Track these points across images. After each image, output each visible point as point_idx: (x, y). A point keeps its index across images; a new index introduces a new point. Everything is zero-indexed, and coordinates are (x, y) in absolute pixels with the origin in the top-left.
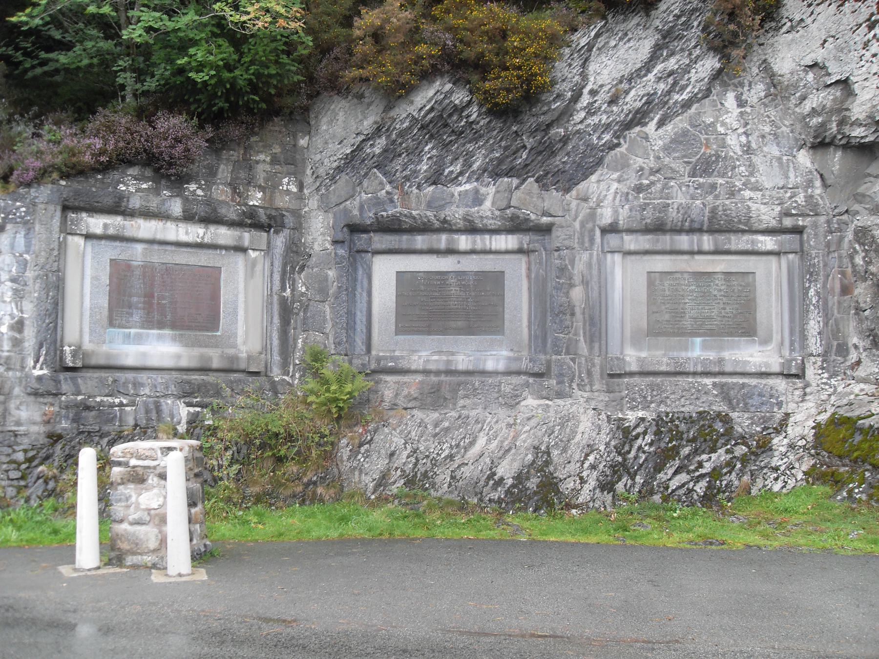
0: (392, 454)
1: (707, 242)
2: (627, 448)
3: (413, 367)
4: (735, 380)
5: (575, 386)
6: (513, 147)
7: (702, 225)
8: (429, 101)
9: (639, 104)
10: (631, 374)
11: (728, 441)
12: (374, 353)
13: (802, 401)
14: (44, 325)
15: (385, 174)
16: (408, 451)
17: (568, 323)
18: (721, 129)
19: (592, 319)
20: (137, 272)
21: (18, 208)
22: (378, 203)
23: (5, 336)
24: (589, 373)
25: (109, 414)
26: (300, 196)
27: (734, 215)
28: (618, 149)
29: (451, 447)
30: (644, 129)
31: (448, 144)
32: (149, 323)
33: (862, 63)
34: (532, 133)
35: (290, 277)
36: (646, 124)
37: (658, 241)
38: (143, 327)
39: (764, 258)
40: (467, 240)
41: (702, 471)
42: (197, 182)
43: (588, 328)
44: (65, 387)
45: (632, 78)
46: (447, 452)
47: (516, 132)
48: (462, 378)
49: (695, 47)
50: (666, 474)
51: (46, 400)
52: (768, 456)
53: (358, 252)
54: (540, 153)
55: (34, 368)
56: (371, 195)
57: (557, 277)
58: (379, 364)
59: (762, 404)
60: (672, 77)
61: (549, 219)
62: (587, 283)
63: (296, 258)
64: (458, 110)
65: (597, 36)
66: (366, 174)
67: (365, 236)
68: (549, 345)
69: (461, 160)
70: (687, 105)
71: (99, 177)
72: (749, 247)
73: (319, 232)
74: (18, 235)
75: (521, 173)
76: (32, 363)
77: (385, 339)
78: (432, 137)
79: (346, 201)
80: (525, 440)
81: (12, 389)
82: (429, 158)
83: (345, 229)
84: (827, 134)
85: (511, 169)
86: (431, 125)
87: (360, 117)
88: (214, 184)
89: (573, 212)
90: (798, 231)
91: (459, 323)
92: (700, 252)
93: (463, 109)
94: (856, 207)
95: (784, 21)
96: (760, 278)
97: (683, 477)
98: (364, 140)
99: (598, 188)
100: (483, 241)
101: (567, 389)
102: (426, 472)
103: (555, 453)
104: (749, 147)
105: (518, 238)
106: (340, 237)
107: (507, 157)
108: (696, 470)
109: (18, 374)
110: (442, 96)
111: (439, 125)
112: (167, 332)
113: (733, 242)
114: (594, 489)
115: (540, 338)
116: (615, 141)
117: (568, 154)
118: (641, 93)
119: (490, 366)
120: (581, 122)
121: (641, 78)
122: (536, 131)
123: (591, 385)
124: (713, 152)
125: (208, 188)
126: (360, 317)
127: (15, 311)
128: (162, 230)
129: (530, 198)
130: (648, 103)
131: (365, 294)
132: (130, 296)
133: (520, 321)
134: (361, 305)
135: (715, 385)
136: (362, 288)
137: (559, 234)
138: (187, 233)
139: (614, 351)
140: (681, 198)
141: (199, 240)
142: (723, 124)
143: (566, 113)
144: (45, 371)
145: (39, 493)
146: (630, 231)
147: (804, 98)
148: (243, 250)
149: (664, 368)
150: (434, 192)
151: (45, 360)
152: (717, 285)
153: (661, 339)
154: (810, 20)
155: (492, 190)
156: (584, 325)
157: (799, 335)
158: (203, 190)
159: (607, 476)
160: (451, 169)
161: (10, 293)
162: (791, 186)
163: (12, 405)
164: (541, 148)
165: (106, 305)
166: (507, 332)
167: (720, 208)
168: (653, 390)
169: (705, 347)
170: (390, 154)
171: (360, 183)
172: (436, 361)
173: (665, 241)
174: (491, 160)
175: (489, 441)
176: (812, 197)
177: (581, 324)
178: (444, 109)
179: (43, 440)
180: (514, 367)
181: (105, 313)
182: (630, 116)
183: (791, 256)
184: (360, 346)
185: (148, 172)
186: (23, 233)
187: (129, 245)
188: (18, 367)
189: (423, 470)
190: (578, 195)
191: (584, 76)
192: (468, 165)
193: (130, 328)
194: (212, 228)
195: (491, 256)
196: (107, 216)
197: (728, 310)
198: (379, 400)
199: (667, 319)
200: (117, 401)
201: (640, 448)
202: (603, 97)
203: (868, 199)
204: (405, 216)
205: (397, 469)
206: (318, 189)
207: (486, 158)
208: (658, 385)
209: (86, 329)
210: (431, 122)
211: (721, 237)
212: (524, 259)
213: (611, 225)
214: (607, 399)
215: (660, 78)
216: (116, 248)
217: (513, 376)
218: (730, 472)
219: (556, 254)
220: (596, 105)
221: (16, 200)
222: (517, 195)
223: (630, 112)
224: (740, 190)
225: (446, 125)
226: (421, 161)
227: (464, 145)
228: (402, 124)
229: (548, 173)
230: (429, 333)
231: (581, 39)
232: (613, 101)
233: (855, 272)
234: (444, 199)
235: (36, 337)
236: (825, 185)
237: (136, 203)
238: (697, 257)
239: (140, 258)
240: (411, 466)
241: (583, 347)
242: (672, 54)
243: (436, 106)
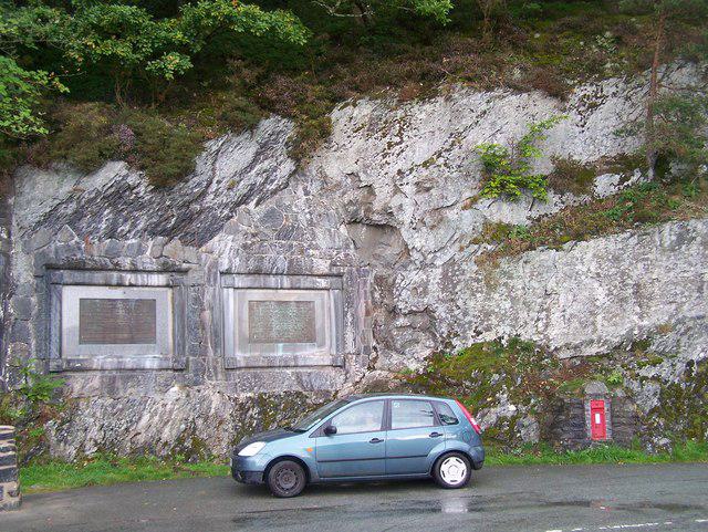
1: (286, 282)
9: (246, 191)
10: (240, 368)
22: (68, 248)
24: (215, 368)
64: (131, 188)
70: (274, 192)
75: (170, 234)
77: (72, 348)
90: (340, 275)
92: (281, 288)
96: (318, 303)
111: (118, 196)
115: (179, 346)
119: (148, 364)
126: (54, 331)
129: (176, 250)
134: (55, 323)
139: (229, 354)
142: (296, 206)
147: (344, 193)
149: (261, 364)
153: (258, 345)
154: (349, 146)
155: (150, 243)
157: (341, 341)
166: (158, 342)
169: (284, 349)
170: (78, 215)
172: (110, 363)
175: (152, 417)
180: (165, 365)
192: (134, 225)
195: (147, 289)
199: (260, 336)
206: (22, 237)
212: (170, 291)
222: (168, 247)
225: (120, 198)
227: (131, 212)
230: (104, 343)
231: (213, 145)
233: (374, 302)
236: (356, 248)
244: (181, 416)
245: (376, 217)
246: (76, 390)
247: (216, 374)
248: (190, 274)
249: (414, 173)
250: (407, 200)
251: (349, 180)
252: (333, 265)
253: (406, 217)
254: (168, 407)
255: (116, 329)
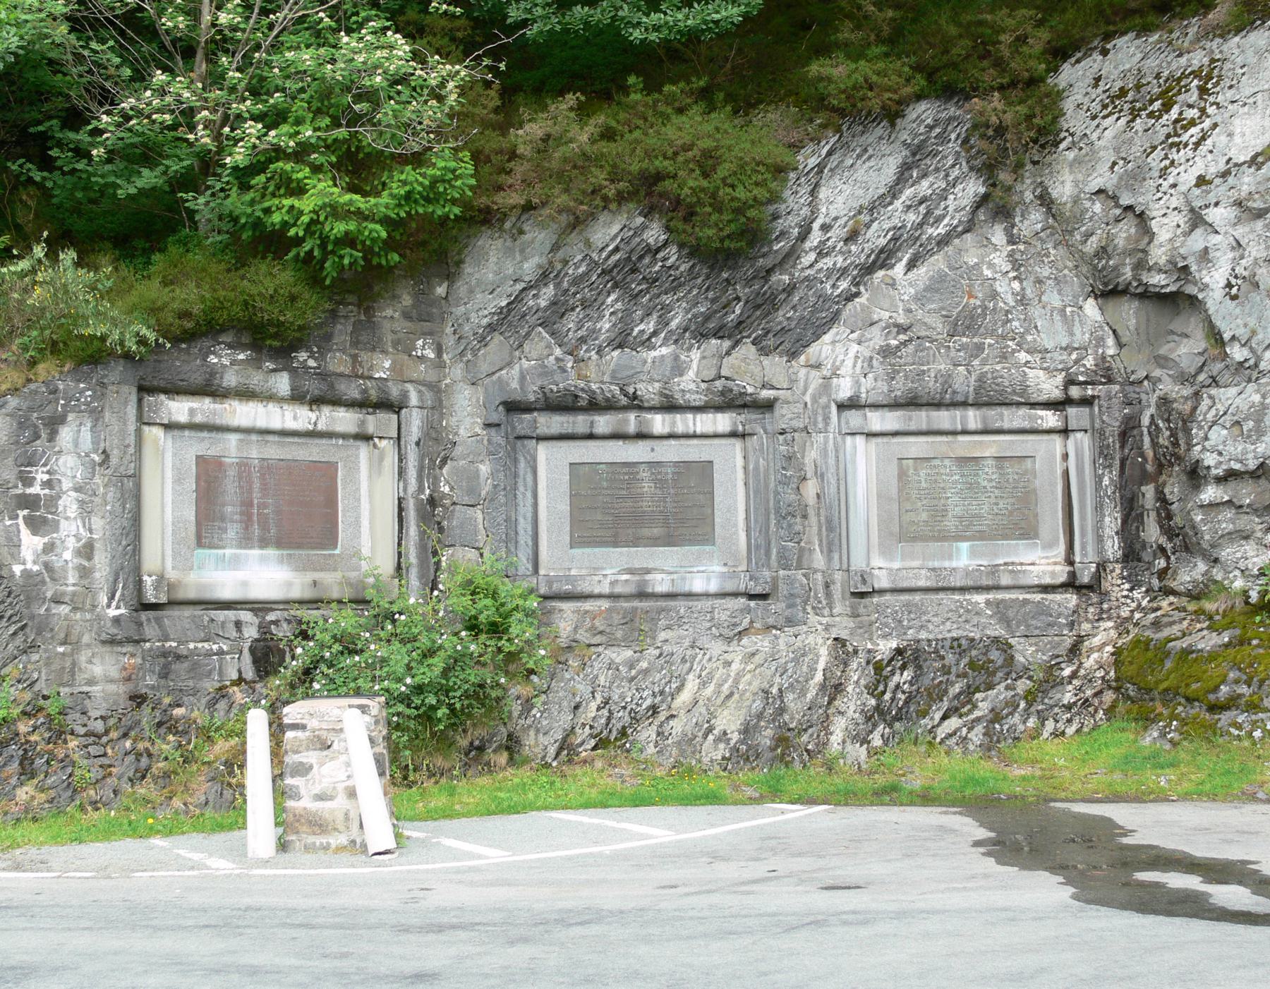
0: (576, 707)
1: (973, 418)
2: (881, 688)
3: (597, 591)
4: (1013, 596)
5: (809, 609)
6: (724, 300)
7: (967, 397)
8: (613, 239)
9: (882, 242)
10: (882, 592)
11: (1008, 674)
12: (542, 572)
13: (1098, 620)
14: (121, 548)
15: (552, 334)
16: (599, 699)
17: (798, 528)
18: (988, 273)
19: (829, 521)
20: (232, 473)
21: (82, 392)
23: (70, 565)
25: (208, 665)
26: (439, 364)
27: (1007, 384)
28: (857, 300)
29: (654, 695)
30: (890, 272)
31: (637, 295)
32: (246, 541)
33: (1159, 195)
34: (748, 282)
35: (429, 473)
36: (892, 267)
37: (910, 419)
38: (240, 547)
39: (1046, 437)
40: (664, 421)
41: (977, 713)
42: (309, 349)
43: (824, 533)
44: (150, 631)
45: (874, 207)
46: (648, 702)
47: (727, 280)
48: (662, 603)
49: (953, 166)
50: (932, 719)
51: (124, 650)
52: (1059, 692)
53: (519, 438)
54: (758, 307)
55: (109, 606)
56: (533, 363)
57: (784, 468)
58: (550, 588)
59: (1049, 625)
60: (924, 205)
61: (771, 392)
62: (822, 475)
63: (437, 450)
65: (830, 154)
66: (528, 334)
67: (527, 416)
68: (774, 557)
69: (655, 316)
70: (943, 241)
71: (184, 346)
72: (1026, 425)
73: (467, 415)
74: (83, 428)
75: (733, 333)
76: (106, 600)
78: (616, 286)
79: (501, 369)
80: (751, 684)
81: (81, 635)
82: (612, 314)
83: (501, 408)
84: (1120, 280)
85: (721, 328)
86: (615, 271)
87: (518, 257)
88: (330, 350)
89: (802, 383)
91: (655, 530)
92: (965, 432)
93: (658, 250)
94: (1157, 373)
95: (1063, 135)
97: (954, 722)
98: (524, 289)
99: (833, 351)
100: (685, 422)
101: (801, 614)
102: (624, 728)
103: (790, 697)
104: (1023, 297)
105: (731, 418)
106: (494, 418)
107: (716, 312)
108: (970, 712)
109: (88, 616)
110: (631, 233)
111: (625, 272)
112: (271, 552)
113: (1006, 419)
114: (844, 742)
115: (759, 549)
116: (854, 290)
117: (794, 308)
118: (886, 226)
119: (698, 585)
120: (811, 266)
121: (885, 207)
122: (754, 278)
123: (831, 609)
124: (978, 303)
125: (321, 357)
126: (524, 526)
127: (81, 530)
128: (264, 414)
129: (748, 367)
130: (895, 239)
131: (529, 494)
132: (224, 505)
133: (736, 525)
134: (525, 509)
135: (988, 603)
136: (525, 486)
137: (784, 412)
138: (295, 418)
139: (858, 563)
140: (942, 366)
141: (311, 427)
142: (991, 265)
143: (792, 255)
144: (122, 611)
145: (131, 774)
146: (875, 406)
148: (367, 438)
149: (922, 583)
150: (619, 358)
151: (123, 595)
152: (987, 474)
153: (919, 546)
156: (820, 530)
158: (316, 359)
159: (858, 724)
160: (642, 327)
161: (75, 507)
162: (1076, 345)
163: (83, 658)
164: (759, 301)
165: (193, 518)
166: (718, 541)
167: (989, 376)
168: (910, 612)
169: (973, 553)
170: (559, 309)
171: (521, 346)
173: (921, 418)
174: (695, 316)
176: (1104, 358)
177: (815, 529)
178: (632, 251)
179: (124, 703)
180: (730, 587)
181: (192, 529)
182: (873, 256)
183: (1079, 435)
184: (524, 565)
185: (246, 339)
186: (89, 425)
187: (220, 435)
188: (88, 607)
189: (619, 726)
190: (807, 360)
191: (814, 213)
192: (663, 322)
193: (224, 548)
194: (326, 410)
195: (695, 441)
196: (191, 398)
197: (1001, 506)
198: (552, 636)
200: (215, 647)
201: (898, 686)
202: (837, 233)
203: (1171, 364)
204: (582, 389)
205: (584, 725)
206: (462, 354)
207: (687, 313)
208: (916, 605)
209: (169, 552)
210: (615, 266)
211: (992, 413)
212: (738, 444)
213: (850, 399)
214: (852, 625)
215: (909, 207)
216: (203, 439)
217: (728, 599)
218: (1011, 714)
219: (781, 438)
220: (829, 243)
221: (79, 381)
223: (873, 251)
224: (1014, 351)
225: (634, 270)
226: (601, 317)
227: (659, 295)
228: (577, 268)
229: (768, 332)
231: (809, 159)
232: (852, 237)
234: (633, 368)
235: (110, 565)
237: (231, 379)
238: (961, 438)
239: (233, 452)
240: (603, 721)
241: (819, 560)
242: (924, 175)
243: (622, 246)
244: (756, 685)
245: (1157, 280)
246: (564, 634)
247: (830, 606)
248: (779, 410)
249: (1231, 180)
250: (1218, 238)
251: (1098, 207)
252: (1070, 382)
253: (1215, 278)
254: (735, 667)
255: (638, 519)
